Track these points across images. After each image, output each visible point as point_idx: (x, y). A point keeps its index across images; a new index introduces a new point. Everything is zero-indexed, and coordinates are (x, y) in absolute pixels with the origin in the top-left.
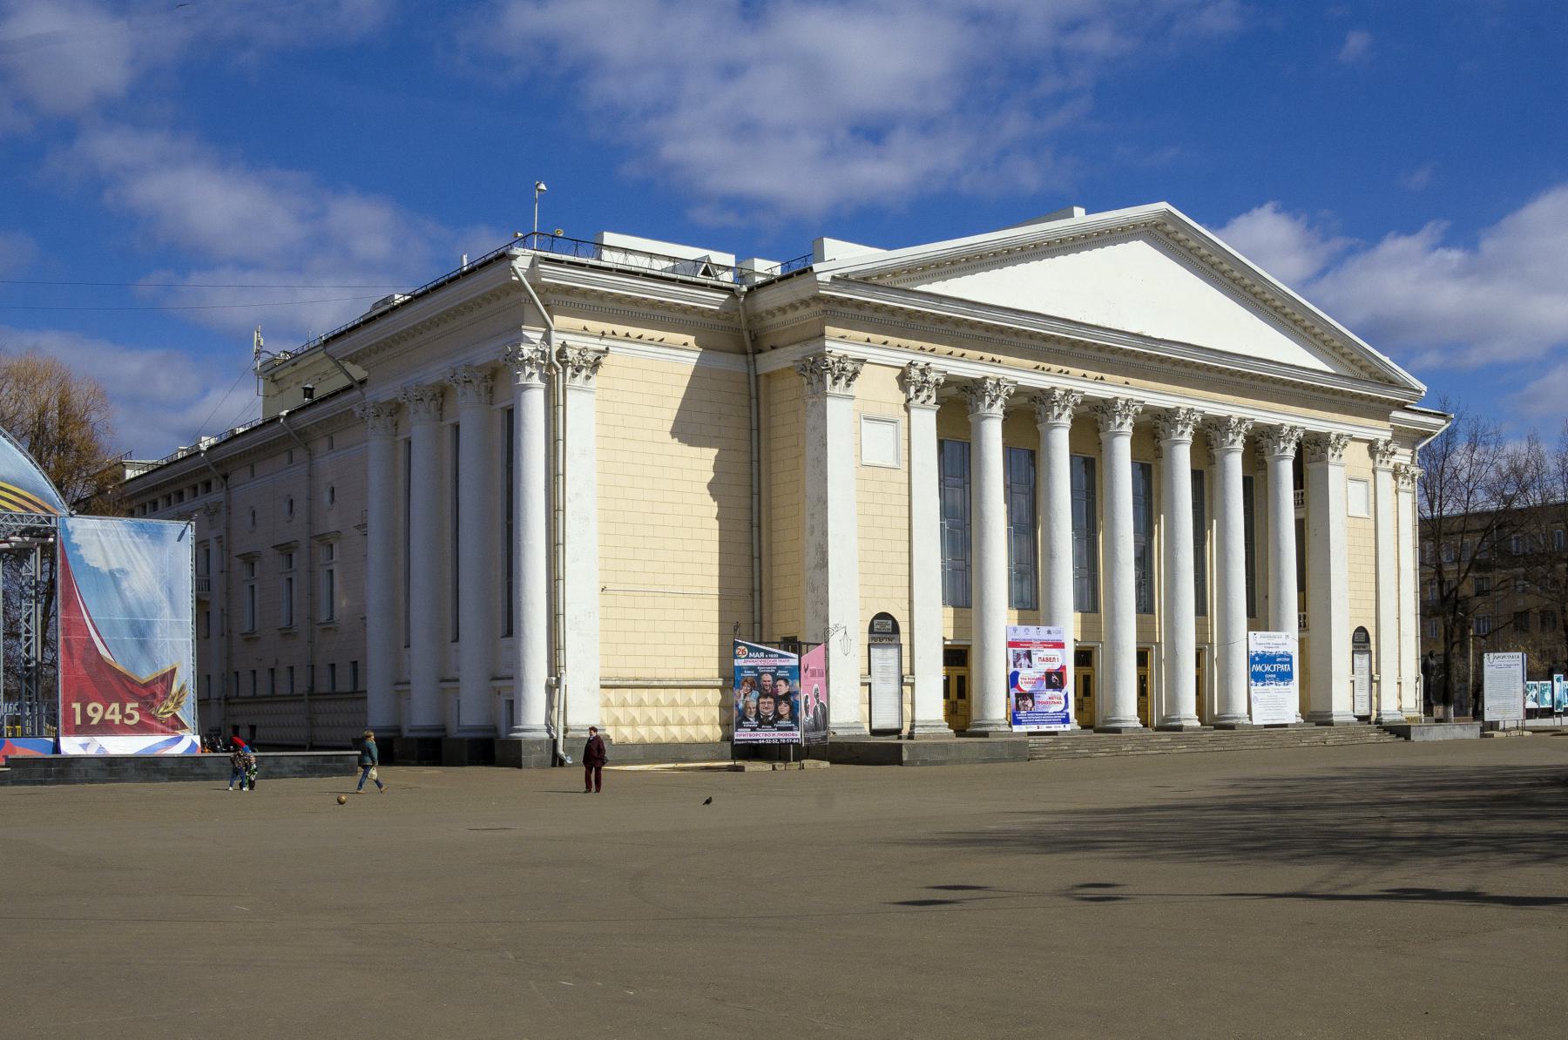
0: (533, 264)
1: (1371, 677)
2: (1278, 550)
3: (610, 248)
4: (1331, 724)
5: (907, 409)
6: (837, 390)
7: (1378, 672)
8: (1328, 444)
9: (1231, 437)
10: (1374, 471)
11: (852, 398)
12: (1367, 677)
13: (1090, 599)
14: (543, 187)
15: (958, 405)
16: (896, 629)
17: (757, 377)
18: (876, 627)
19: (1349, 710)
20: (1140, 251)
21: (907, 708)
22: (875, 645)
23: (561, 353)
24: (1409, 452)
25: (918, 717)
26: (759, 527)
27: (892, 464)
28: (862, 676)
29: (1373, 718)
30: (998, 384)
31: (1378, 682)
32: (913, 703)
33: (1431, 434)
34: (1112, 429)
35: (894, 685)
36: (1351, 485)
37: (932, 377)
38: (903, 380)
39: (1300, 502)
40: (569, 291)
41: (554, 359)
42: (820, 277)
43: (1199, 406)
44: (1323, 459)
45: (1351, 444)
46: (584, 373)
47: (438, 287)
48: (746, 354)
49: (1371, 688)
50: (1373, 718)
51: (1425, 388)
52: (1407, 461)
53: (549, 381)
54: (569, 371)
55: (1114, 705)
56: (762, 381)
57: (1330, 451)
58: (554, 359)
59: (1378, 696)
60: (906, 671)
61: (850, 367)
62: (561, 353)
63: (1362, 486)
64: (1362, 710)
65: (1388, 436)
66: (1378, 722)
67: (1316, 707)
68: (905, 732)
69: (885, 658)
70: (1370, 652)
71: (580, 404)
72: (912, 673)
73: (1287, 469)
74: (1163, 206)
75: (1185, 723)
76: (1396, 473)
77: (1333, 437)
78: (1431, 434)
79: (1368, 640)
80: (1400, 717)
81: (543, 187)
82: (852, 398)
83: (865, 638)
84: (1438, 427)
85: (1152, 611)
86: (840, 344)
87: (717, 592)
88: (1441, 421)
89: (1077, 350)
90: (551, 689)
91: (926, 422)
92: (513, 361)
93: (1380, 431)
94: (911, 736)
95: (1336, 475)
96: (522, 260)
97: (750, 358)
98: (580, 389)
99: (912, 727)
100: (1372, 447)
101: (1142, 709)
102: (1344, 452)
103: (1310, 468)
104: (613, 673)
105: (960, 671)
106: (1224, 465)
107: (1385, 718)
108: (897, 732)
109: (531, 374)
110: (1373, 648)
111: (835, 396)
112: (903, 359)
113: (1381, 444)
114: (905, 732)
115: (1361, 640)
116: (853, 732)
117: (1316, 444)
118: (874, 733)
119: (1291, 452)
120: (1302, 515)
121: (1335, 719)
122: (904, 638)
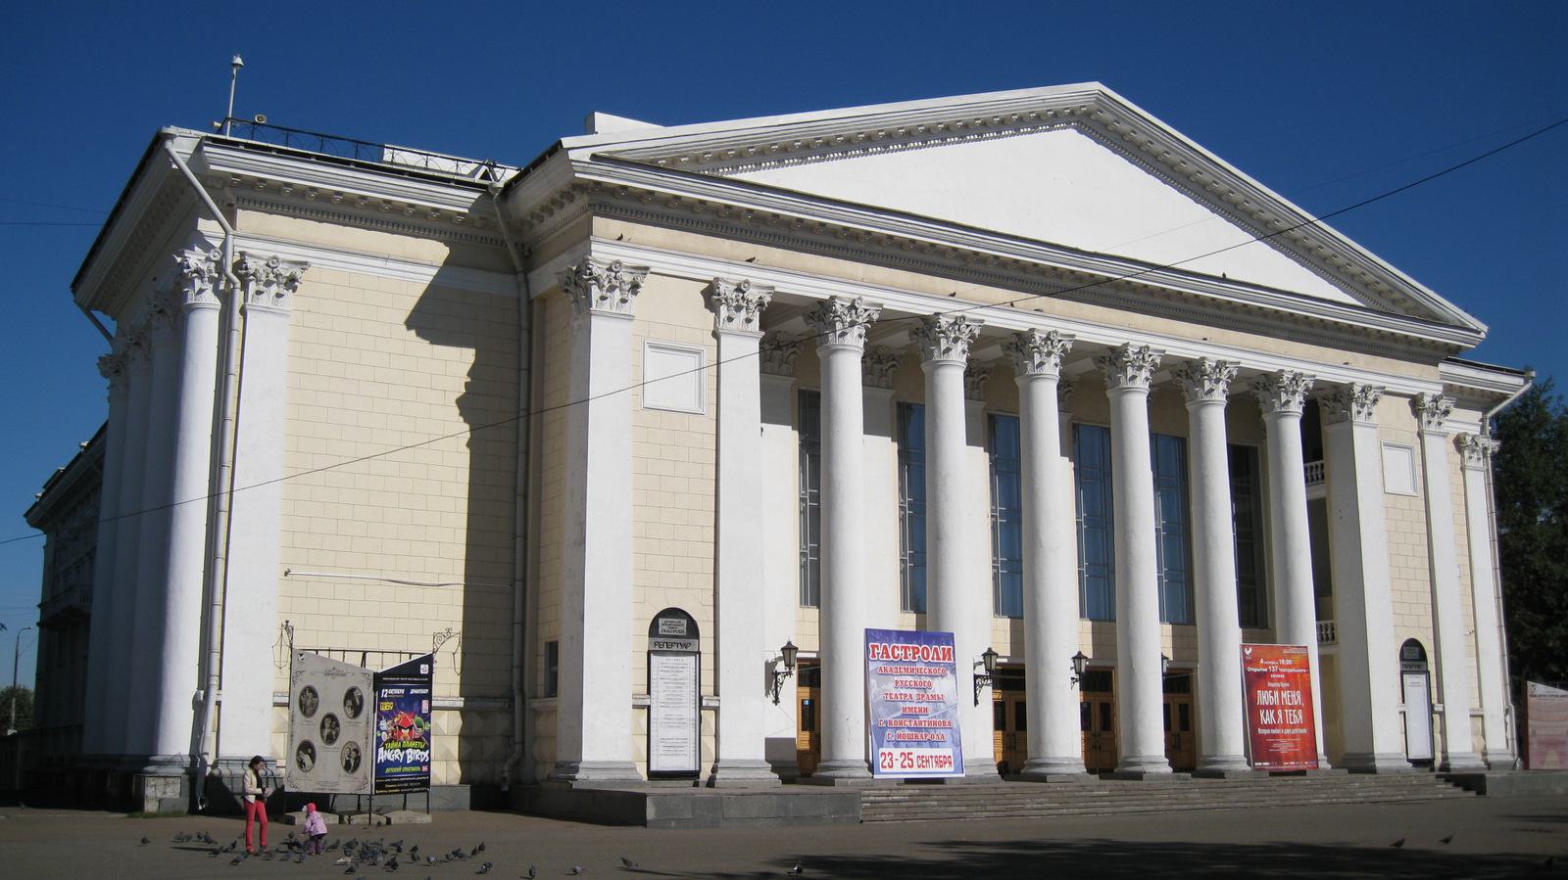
0: (199, 148)
1: (1431, 707)
2: (1284, 536)
3: (548, 209)
4: (1373, 771)
5: (716, 335)
6: (606, 306)
7: (1441, 700)
8: (1351, 398)
9: (1207, 385)
10: (1420, 435)
11: (630, 318)
12: (1425, 708)
13: (1014, 592)
14: (238, 60)
15: (793, 343)
16: (693, 631)
17: (530, 302)
18: (662, 628)
19: (1399, 748)
20: (1069, 141)
21: (708, 742)
22: (657, 653)
23: (239, 266)
24: (1479, 415)
25: (722, 756)
26: (525, 497)
27: (694, 407)
28: (635, 696)
29: (1438, 763)
30: (853, 307)
31: (1442, 714)
32: (717, 736)
33: (1504, 397)
34: (1030, 371)
35: (689, 712)
36: (1388, 453)
37: (753, 294)
38: (711, 296)
39: (1313, 477)
40: (252, 184)
41: (229, 270)
42: (572, 155)
43: (1156, 343)
44: (1347, 420)
45: (1385, 400)
46: (274, 289)
47: (126, 195)
48: (515, 272)
49: (1432, 721)
50: (1438, 763)
51: (1485, 328)
52: (1475, 430)
53: (226, 298)
54: (253, 287)
55: (1215, 739)
56: (536, 305)
57: (1355, 408)
58: (229, 270)
59: (1443, 733)
60: (1434, 701)
61: (628, 278)
62: (239, 266)
63: (1405, 455)
64: (1420, 749)
65: (1438, 390)
66: (1445, 767)
67: (1352, 747)
68: (704, 776)
69: (674, 670)
70: (1427, 672)
71: (268, 331)
72: (716, 693)
73: (1292, 432)
74: (1095, 86)
75: (1150, 769)
76: (1459, 443)
77: (1357, 389)
78: (1504, 397)
79: (1423, 657)
80: (1477, 762)
81: (238, 60)
82: (630, 318)
83: (645, 643)
84: (1515, 388)
85: (1112, 620)
86: (612, 244)
87: (462, 580)
88: (1519, 381)
89: (1122, 294)
90: (200, 707)
91: (744, 350)
92: (182, 279)
93: (1427, 380)
94: (711, 783)
95: (1365, 439)
96: (182, 145)
97: (521, 277)
98: (266, 311)
99: (714, 770)
100: (1415, 403)
101: (1173, 748)
102: (1374, 409)
103: (1329, 431)
104: (637, 692)
105: (1182, 698)
106: (1199, 422)
107: (1454, 764)
108: (692, 775)
109: (201, 291)
110: (1432, 667)
111: (603, 315)
112: (709, 271)
113: (1427, 400)
114: (704, 776)
115: (1413, 657)
116: (619, 775)
117: (1336, 399)
118: (654, 776)
119: (1296, 407)
120: (1320, 492)
121: (1379, 764)
122: (705, 644)
